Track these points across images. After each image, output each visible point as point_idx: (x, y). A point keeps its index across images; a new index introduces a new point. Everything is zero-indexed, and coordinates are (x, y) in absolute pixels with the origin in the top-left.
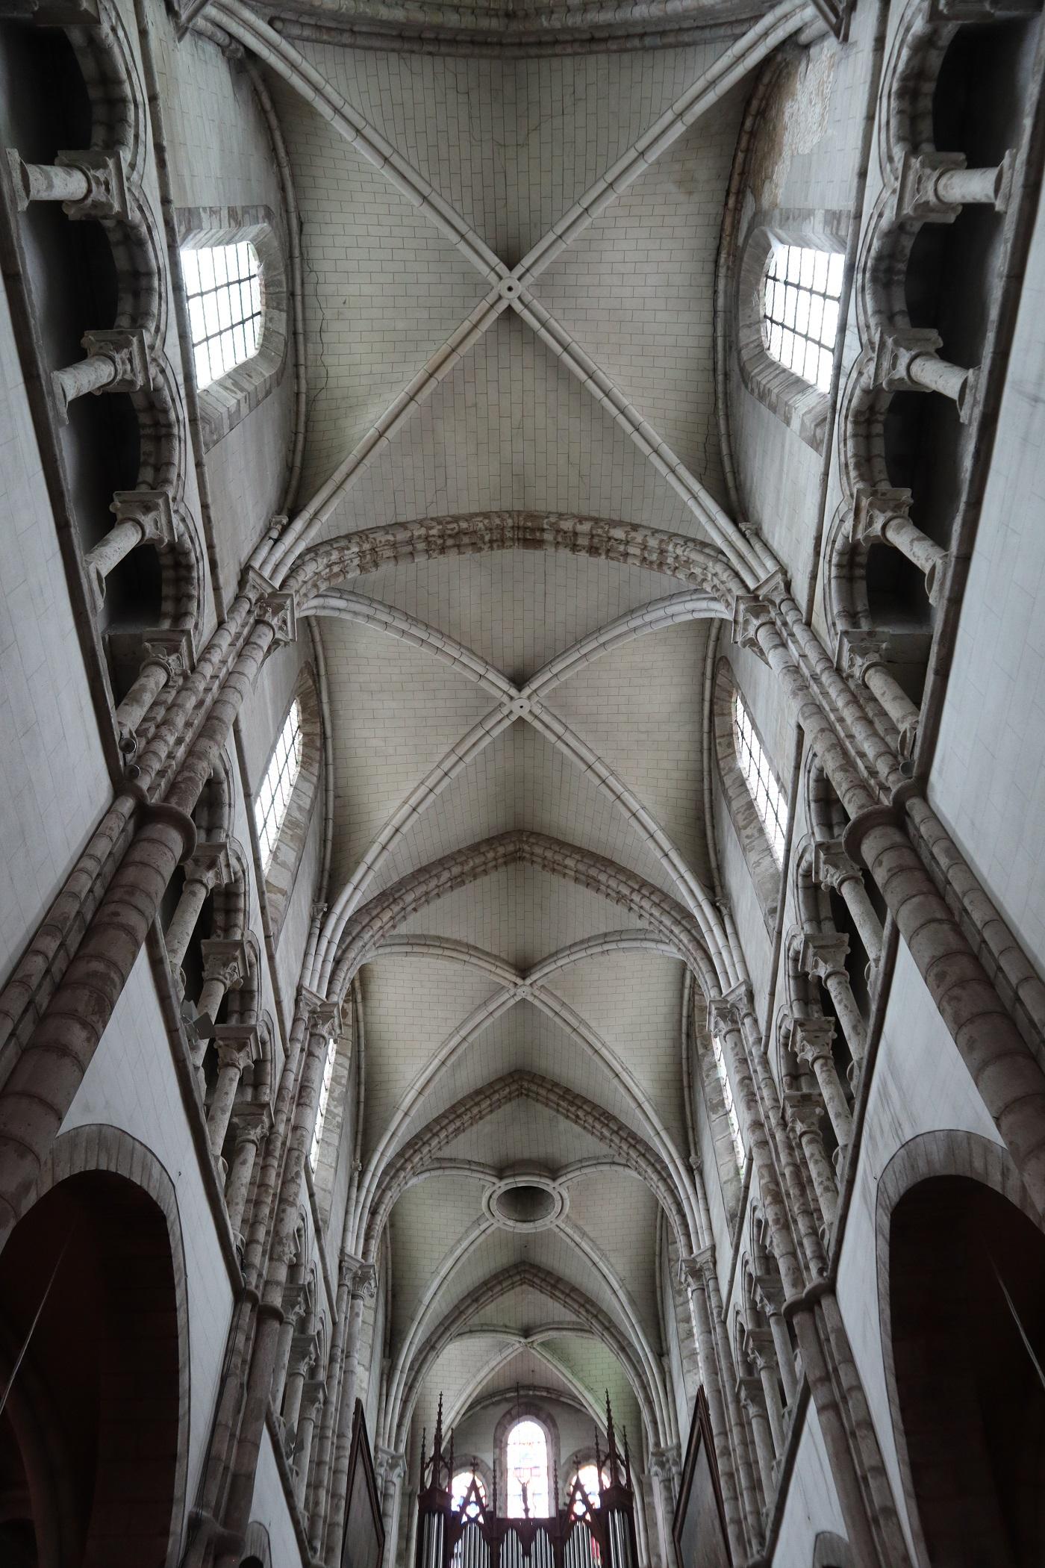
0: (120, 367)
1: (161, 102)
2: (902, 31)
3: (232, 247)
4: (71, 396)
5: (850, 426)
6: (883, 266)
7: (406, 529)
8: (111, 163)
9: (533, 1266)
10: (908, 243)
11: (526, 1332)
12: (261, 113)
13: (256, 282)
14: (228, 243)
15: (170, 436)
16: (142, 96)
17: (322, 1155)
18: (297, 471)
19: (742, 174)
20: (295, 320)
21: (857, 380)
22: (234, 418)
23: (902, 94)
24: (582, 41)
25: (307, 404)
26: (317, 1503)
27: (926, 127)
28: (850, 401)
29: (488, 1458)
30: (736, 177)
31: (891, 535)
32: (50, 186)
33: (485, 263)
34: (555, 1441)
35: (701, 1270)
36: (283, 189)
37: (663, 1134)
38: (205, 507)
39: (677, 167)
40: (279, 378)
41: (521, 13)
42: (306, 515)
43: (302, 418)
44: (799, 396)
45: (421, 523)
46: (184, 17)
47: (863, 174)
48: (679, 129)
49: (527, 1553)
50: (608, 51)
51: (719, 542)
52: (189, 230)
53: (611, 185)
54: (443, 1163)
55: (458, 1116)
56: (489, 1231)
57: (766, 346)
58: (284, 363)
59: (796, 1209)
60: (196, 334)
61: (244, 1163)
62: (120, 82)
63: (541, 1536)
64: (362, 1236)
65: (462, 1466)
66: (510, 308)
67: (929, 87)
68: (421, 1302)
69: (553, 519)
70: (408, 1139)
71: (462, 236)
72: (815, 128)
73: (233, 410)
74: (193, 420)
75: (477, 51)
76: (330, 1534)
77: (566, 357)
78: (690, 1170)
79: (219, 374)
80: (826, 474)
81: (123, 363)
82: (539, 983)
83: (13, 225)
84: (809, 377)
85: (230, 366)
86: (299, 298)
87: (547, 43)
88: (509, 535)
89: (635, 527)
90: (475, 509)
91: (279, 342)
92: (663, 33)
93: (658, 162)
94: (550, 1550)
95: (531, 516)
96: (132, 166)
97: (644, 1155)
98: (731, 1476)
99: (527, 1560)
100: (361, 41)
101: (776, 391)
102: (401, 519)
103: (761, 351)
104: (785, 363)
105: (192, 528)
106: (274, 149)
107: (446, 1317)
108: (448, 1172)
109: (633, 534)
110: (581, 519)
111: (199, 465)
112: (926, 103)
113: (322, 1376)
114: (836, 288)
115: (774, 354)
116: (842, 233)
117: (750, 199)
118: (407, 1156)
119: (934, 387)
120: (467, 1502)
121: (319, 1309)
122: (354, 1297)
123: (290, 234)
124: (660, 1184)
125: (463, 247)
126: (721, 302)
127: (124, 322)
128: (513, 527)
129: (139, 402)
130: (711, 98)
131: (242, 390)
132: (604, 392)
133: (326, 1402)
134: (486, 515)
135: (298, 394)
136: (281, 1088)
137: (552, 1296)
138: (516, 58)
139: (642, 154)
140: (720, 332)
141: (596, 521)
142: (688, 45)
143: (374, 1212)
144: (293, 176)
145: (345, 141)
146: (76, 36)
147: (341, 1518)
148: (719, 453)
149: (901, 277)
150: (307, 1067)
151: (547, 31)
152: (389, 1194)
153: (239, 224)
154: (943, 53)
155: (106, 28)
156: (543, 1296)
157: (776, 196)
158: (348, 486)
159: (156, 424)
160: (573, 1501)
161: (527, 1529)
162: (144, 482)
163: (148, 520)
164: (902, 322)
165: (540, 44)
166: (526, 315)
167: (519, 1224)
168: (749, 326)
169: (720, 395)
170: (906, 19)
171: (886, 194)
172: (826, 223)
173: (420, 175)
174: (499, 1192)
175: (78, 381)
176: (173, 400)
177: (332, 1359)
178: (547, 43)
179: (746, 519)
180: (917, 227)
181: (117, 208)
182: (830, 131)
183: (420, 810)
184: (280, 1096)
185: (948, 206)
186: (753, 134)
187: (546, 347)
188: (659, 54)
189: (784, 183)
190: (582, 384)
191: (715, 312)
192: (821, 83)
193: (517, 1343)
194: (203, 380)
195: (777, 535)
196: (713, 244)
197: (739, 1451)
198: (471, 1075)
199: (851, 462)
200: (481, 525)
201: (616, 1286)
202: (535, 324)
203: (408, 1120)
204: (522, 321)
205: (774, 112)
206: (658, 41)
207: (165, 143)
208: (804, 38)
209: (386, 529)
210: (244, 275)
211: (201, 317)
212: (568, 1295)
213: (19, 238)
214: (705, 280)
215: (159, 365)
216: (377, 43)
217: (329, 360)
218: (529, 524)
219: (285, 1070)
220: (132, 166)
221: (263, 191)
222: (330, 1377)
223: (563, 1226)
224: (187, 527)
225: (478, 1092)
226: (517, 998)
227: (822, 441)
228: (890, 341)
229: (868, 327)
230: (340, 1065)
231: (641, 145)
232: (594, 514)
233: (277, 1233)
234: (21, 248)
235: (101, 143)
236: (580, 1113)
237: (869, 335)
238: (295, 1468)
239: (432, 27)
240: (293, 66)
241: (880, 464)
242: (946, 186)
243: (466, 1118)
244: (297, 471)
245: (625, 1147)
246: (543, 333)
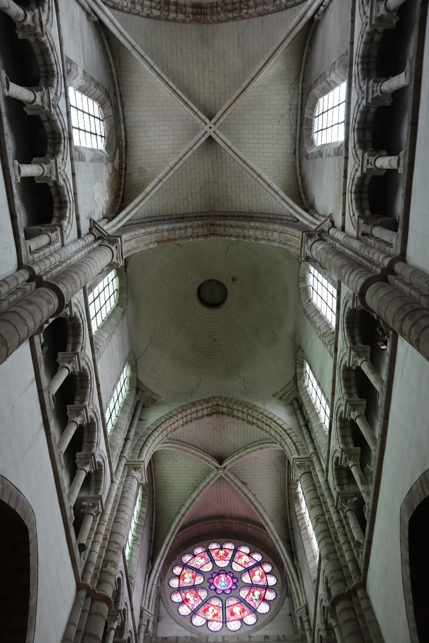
0: (378, 88)
1: (342, 193)
2: (71, 222)
3: (323, 143)
4: (403, 74)
5: (55, 69)
6: (57, 140)
7: (258, 13)
8: (365, 171)
10: (49, 149)
12: (305, 192)
13: (315, 130)
14: (324, 144)
15: (363, 57)
16: (348, 195)
18: (307, 44)
19: (121, 176)
20: (301, 114)
21: (57, 91)
22: (332, 68)
23: (66, 202)
24: (186, 218)
25: (300, 77)
27: (53, 192)
28: (58, 81)
30: (123, 174)
31: (21, 12)
32: (390, 161)
33: (221, 138)
36: (300, 166)
38: (353, 21)
39: (147, 177)
40: (311, 88)
41: (208, 225)
42: (305, 20)
43: (302, 70)
44: (82, 84)
45: (251, 16)
46: (329, 220)
47: (73, 174)
48: (147, 190)
50: (176, 215)
51: (106, 9)
52: (339, 148)
53: (172, 169)
57: (100, 108)
58: (308, 95)
60: (343, 107)
62: (355, 199)
66: (210, 120)
67: (56, 205)
69: (188, 20)
71: (230, 148)
72: (96, 191)
73: (333, 72)
74: (351, 65)
75: (224, 214)
77: (186, 99)
79: (337, 90)
80: (61, 45)
81: (377, 91)
83: (408, 147)
84: (78, 94)
85: (331, 94)
86: (298, 124)
87: (199, 217)
88: (209, 11)
89: (148, 16)
90: (225, 24)
91: (309, 105)
92: (157, 221)
93: (154, 178)
95: (197, 21)
96: (357, 170)
100: (267, 216)
101: (92, 87)
102: (260, 18)
103: (102, 105)
104: (90, 101)
105: (361, 9)
106: (302, 180)
109: (149, 12)
110: (174, 20)
111: (352, 43)
112: (56, 199)
114: (75, 132)
115: (96, 106)
116: (77, 153)
117: (117, 167)
119: (22, 88)
123: (299, 149)
125: (230, 144)
126: (122, 126)
127: (373, 110)
128: (207, 15)
129: (374, 74)
130: (137, 201)
131: (327, 82)
132: (168, 84)
134: (220, 21)
135: (303, 81)
138: (210, 212)
139: (160, 181)
140: (121, 113)
141: (167, 20)
142: (148, 217)
144: (296, 171)
145: (274, 183)
146: (368, 213)
148: (113, 57)
149: (49, 136)
151: (199, 220)
153: (319, 152)
154: (54, 216)
155: (356, 215)
157: (106, 167)
158: (284, 35)
159: (368, 63)
162: (379, 33)
163: (382, 11)
164: (43, 117)
165: (201, 216)
166: (203, 117)
168: (109, 116)
169: (117, 85)
170: (70, 225)
171: (63, 167)
172: (84, 157)
173: (247, 171)
175: (399, 81)
176: (358, 75)
178: (199, 217)
179: (95, 22)
180: (47, 155)
181: (366, 154)
182: (90, 190)
185: (36, 163)
186: (119, 190)
187: (194, 104)
188: (158, 214)
189: (105, 172)
190: (178, 87)
191: (124, 122)
192: (96, 206)
194: (344, 86)
195: (78, 12)
196: (129, 149)
199: (50, 52)
200: (222, 15)
202: (199, 113)
204: (205, 115)
205: (113, 197)
206: (158, 218)
207: (343, 179)
208: (106, 220)
209: (268, 13)
210: (320, 133)
211: (340, 114)
213: (407, 140)
214: (130, 135)
215: (362, 90)
216: (260, 215)
217: (288, 97)
218: (199, 17)
220: (357, 170)
221: (308, 165)
224: (364, 9)
227: (67, 62)
228: (46, 108)
229: (57, 115)
231: (161, 184)
232: (168, 23)
234: (407, 136)
235: (367, 179)
237: (56, 111)
239: (241, 220)
240: (292, 207)
241: (37, 51)
242: (40, 170)
244: (307, 44)
246: (196, 109)
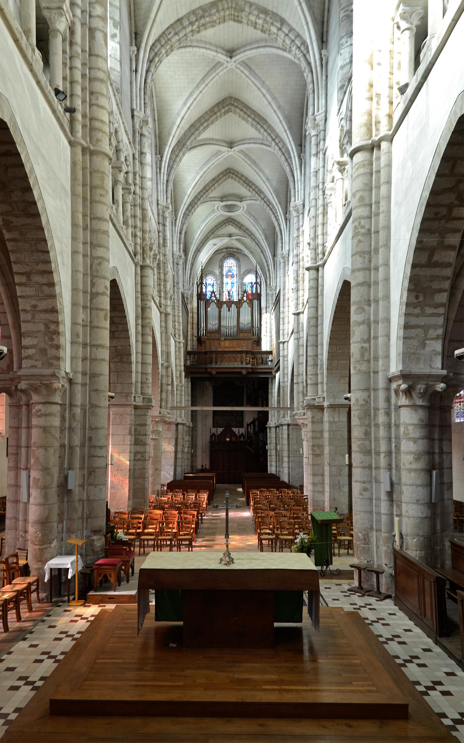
49: (229, 310)
63: (233, 306)
68: (194, 237)
76: (179, 332)
78: (286, 219)
82: (240, 60)
120: (211, 296)
143: (181, 233)
156: (239, 184)
160: (243, 296)
161: (229, 303)
183: (191, 108)
193: (226, 152)
203: (179, 129)
226: (228, 68)
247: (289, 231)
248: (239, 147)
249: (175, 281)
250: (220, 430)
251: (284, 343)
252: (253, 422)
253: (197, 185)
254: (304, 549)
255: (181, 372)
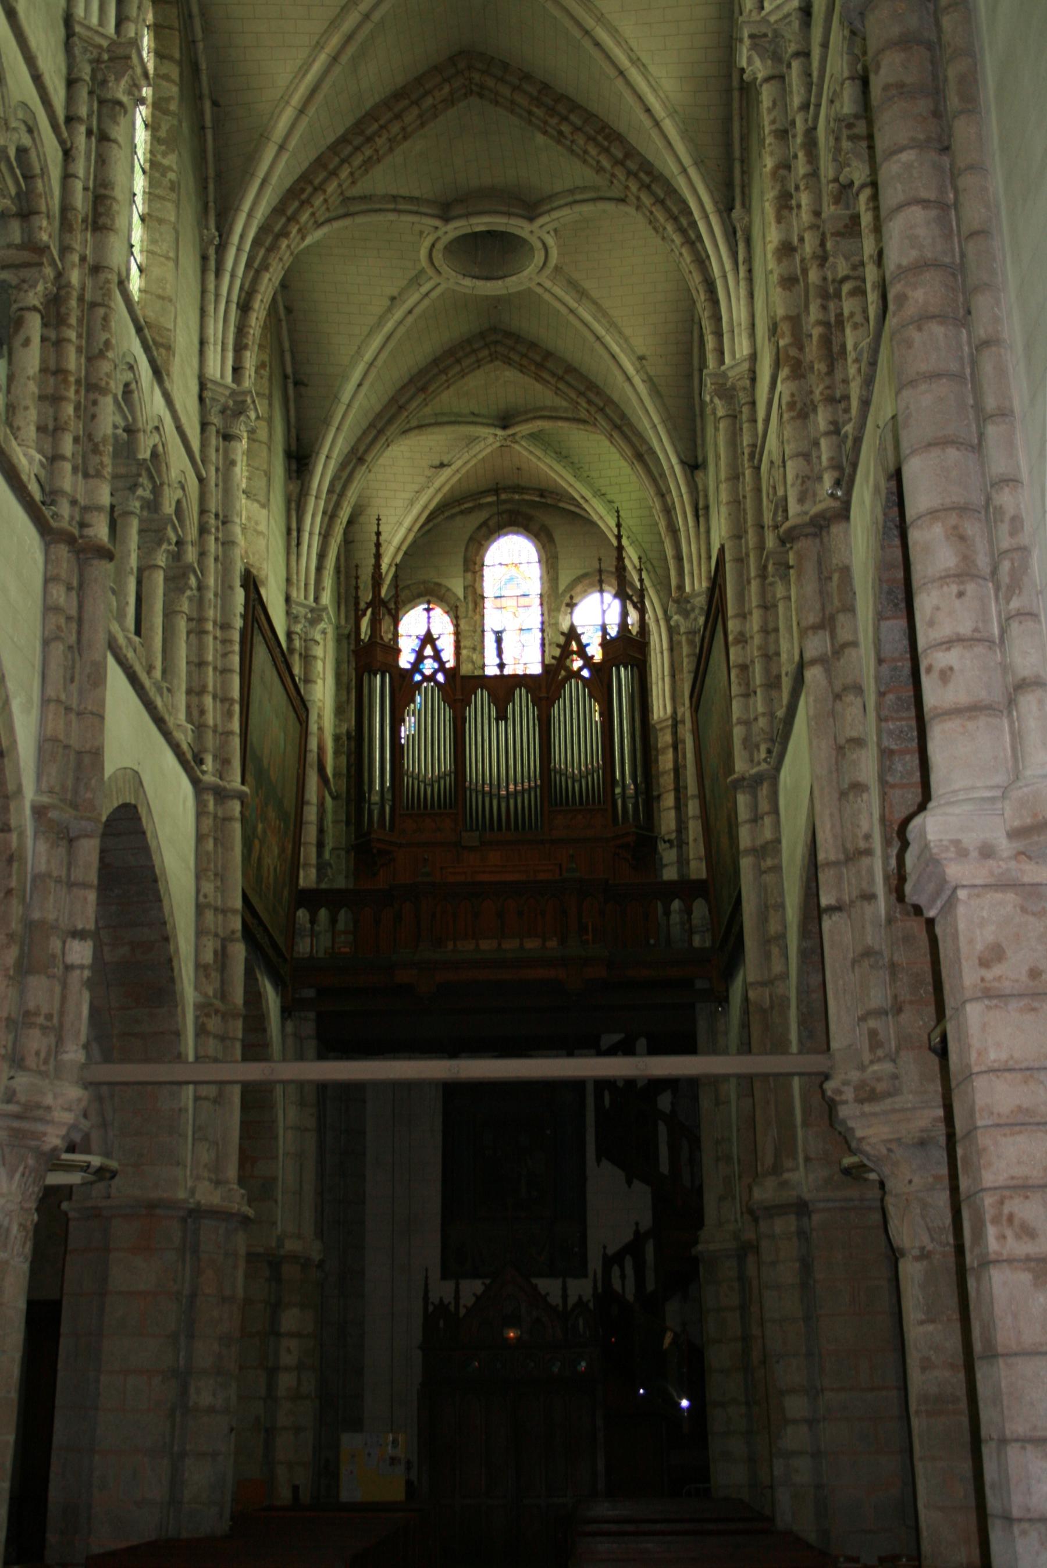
9: (508, 334)
11: (505, 420)
17: (153, 241)
26: (202, 712)
29: (457, 586)
34: (550, 562)
35: (733, 388)
37: (692, 172)
49: (502, 716)
54: (351, 206)
55: (369, 139)
56: (434, 294)
59: (817, 392)
61: (27, 342)
63: (521, 701)
64: (230, 347)
65: (411, 601)
70: (288, 183)
76: (224, 745)
78: (731, 234)
94: (533, 712)
97: (662, 202)
98: (744, 668)
99: (502, 724)
107: (379, 416)
108: (360, 219)
113: (191, 555)
118: (289, 212)
120: (420, 657)
121: (174, 474)
122: (227, 437)
124: (684, 251)
130: (246, 206)
133: (201, 587)
136: (66, 208)
137: (538, 378)
143: (245, 308)
147: (236, 725)
150: (102, 161)
152: (267, 276)
161: (505, 686)
167: (480, 283)
174: (445, 241)
177: (203, 530)
184: (66, 225)
197: (757, 640)
198: (381, 73)
201: (631, 370)
212: (561, 379)
219: (67, 177)
222: (202, 554)
223: (548, 284)
225: (398, 95)
230: (166, 77)
233: (90, 437)
236: (565, 128)
238: (165, 685)
243: (380, 141)
245: (634, 187)
247: (750, 280)
248: (555, 215)
249: (212, 506)
250: (472, 1288)
251: (758, 780)
252: (634, 1248)
253: (319, 97)
254: (376, 676)
255: (225, 941)
